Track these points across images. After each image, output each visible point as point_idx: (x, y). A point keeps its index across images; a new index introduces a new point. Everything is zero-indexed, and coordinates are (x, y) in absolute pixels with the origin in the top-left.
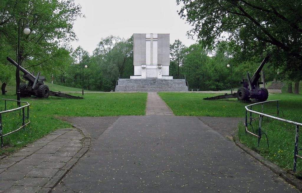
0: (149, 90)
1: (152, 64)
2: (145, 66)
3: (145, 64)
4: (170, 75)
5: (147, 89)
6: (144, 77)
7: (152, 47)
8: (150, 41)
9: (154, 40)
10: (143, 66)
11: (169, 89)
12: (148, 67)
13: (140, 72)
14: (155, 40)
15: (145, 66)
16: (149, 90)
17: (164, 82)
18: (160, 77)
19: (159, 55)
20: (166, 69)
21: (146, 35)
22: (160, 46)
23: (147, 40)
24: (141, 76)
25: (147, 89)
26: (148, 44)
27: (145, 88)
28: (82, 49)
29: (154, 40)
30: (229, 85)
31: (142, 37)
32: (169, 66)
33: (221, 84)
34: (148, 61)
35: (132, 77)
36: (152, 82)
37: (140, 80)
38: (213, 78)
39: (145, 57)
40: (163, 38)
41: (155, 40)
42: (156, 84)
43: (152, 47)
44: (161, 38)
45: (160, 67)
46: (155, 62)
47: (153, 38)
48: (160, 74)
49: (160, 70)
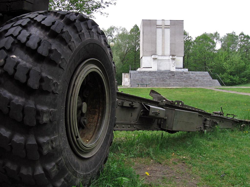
0: (172, 84)
1: (163, 55)
2: (156, 57)
3: (155, 54)
4: (184, 68)
5: (170, 84)
6: (154, 68)
7: (163, 35)
8: (161, 29)
9: (166, 27)
10: (153, 56)
11: (197, 83)
12: (160, 58)
13: (147, 63)
14: (167, 27)
15: (156, 57)
16: (172, 84)
17: (184, 75)
18: (173, 69)
19: (171, 44)
20: (180, 60)
21: (157, 21)
22: (172, 35)
23: (158, 27)
24: (151, 68)
25: (170, 84)
26: (159, 31)
27: (166, 82)
28: (140, 47)
29: (166, 27)
30: (245, 79)
31: (149, 24)
32: (183, 57)
33: (236, 78)
34: (159, 52)
35: (139, 70)
36: (170, 74)
37: (150, 72)
38: (229, 71)
39: (156, 46)
40: (177, 25)
41: (167, 27)
42: (176, 77)
43: (163, 35)
44: (173, 25)
45: (174, 57)
46: (168, 52)
47: (165, 25)
48: (173, 66)
49: (174, 62)
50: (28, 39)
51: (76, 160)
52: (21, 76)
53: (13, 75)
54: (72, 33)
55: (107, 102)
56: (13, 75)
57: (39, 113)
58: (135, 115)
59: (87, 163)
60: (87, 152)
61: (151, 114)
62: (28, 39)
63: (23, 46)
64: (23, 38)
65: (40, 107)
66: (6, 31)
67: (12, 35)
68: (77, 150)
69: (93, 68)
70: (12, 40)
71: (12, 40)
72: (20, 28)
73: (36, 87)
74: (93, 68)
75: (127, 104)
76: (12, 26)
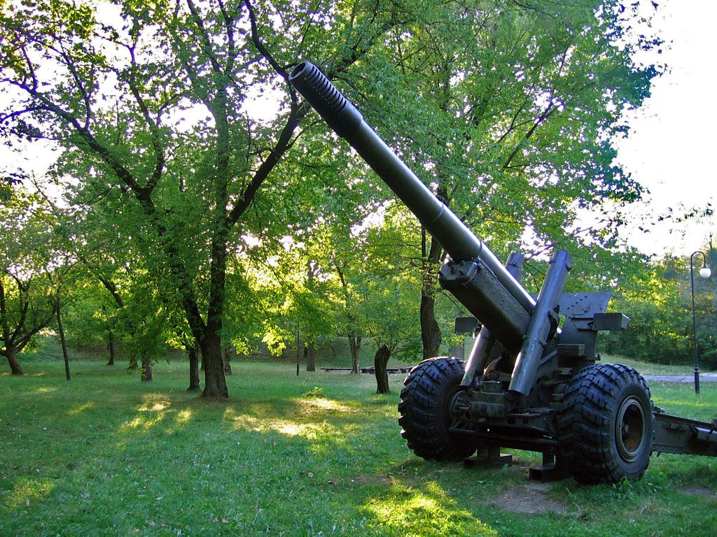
50: (598, 382)
51: (625, 464)
52: (595, 400)
53: (591, 400)
54: (621, 379)
55: (514, 371)
56: (591, 400)
57: (603, 419)
58: (683, 438)
59: (630, 465)
60: (631, 458)
61: (699, 437)
62: (598, 382)
63: (596, 386)
64: (595, 381)
65: (604, 417)
66: (585, 376)
67: (588, 379)
68: (624, 457)
69: (632, 401)
70: (589, 382)
71: (589, 382)
72: (593, 376)
73: (603, 406)
74: (632, 401)
75: (674, 426)
76: (588, 374)
